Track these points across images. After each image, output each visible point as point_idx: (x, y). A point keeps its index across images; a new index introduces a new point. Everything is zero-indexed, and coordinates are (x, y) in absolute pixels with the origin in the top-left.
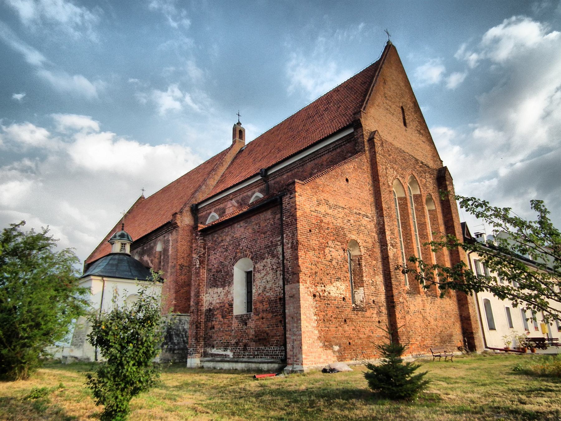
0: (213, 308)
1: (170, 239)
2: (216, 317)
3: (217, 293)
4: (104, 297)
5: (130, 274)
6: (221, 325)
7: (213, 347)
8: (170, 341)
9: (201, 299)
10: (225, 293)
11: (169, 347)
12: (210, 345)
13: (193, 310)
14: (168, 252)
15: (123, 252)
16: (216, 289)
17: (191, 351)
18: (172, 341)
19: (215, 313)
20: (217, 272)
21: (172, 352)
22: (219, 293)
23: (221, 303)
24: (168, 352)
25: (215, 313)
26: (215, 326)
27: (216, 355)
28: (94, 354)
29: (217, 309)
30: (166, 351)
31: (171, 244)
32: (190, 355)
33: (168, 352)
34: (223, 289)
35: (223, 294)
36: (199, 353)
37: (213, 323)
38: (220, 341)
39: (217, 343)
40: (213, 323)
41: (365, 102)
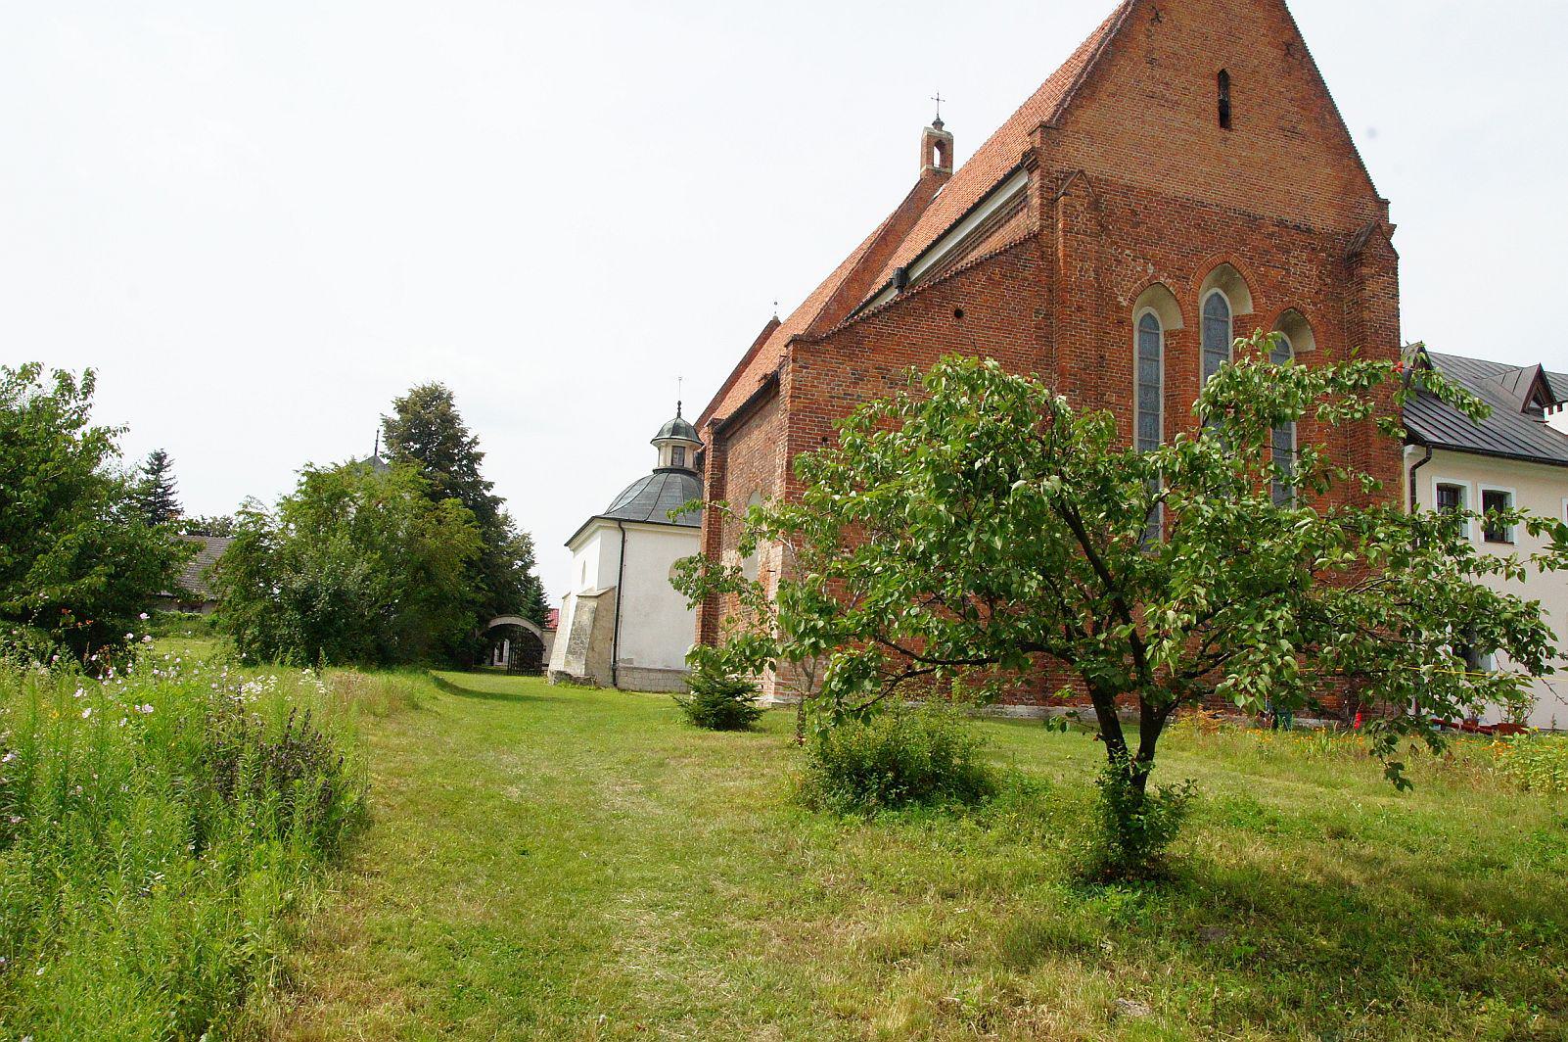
15: (677, 464)
28: (611, 673)
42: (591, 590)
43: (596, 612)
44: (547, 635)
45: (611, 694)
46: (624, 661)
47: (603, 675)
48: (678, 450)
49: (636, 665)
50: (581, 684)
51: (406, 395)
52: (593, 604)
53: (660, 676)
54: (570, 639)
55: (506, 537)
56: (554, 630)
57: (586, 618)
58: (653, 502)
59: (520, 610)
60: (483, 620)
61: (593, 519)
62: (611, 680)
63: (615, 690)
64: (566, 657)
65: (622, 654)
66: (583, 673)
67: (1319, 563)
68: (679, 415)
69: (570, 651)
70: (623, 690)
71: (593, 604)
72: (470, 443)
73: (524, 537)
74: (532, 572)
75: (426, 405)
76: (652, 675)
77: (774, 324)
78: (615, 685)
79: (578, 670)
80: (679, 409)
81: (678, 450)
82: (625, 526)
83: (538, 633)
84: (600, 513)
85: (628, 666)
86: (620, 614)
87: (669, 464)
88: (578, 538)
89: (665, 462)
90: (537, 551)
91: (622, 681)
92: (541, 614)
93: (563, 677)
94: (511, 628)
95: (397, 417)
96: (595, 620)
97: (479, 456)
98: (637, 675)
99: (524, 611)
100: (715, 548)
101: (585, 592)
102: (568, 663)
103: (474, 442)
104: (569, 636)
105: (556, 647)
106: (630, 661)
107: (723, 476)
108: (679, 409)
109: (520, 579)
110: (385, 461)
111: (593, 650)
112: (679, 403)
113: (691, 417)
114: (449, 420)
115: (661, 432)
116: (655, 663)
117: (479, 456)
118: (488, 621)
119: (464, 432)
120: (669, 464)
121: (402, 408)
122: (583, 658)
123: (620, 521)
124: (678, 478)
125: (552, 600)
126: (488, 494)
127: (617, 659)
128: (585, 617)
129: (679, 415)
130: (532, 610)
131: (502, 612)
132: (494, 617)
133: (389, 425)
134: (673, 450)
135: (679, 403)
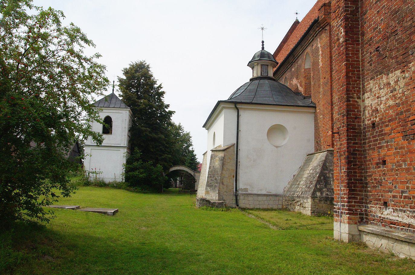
0: (381, 119)
1: (319, 45)
2: (387, 138)
3: (389, 84)
4: (240, 129)
5: (271, 99)
6: (403, 156)
7: (386, 204)
8: (326, 186)
9: (354, 105)
10: (407, 80)
11: (324, 195)
12: (380, 200)
13: (338, 128)
14: (318, 65)
15: (265, 75)
16: (384, 77)
17: (339, 209)
18: (328, 186)
19: (387, 130)
20: (386, 38)
21: (328, 202)
22: (392, 83)
23: (397, 105)
24: (322, 202)
25: (387, 130)
26: (388, 159)
27: (392, 223)
28: (234, 198)
29: (389, 121)
30: (320, 201)
31: (320, 53)
32: (338, 216)
33: (322, 202)
34: (403, 72)
35: (402, 83)
36: (356, 214)
37: (383, 152)
38: (402, 192)
39: (394, 197)
40: (383, 152)
41: (395, 221)
42: (220, 146)
43: (223, 160)
44: (197, 174)
45: (236, 214)
46: (242, 190)
47: (230, 200)
48: (264, 67)
49: (249, 192)
50: (217, 207)
51: (128, 67)
52: (221, 155)
53: (265, 198)
54: (208, 177)
55: (180, 135)
56: (200, 172)
57: (217, 164)
58: (253, 94)
59: (185, 164)
60: (166, 169)
61: (219, 103)
62: (234, 202)
63: (237, 209)
64: (206, 189)
65: (241, 186)
66: (217, 198)
67: (16, 194)
68: (263, 48)
69: (209, 185)
70: (243, 209)
71: (221, 155)
72: (158, 87)
73: (188, 134)
74: (190, 148)
75: (136, 71)
76: (260, 198)
77: (297, 23)
78: (238, 205)
79: (214, 197)
80: (263, 45)
81: (264, 67)
82: (238, 106)
83: (192, 173)
84: (226, 98)
85: (245, 193)
86: (238, 161)
87: (259, 75)
88: (211, 119)
89: (257, 74)
90: (193, 140)
91: (242, 203)
92: (195, 166)
93: (206, 203)
94: (212, 168)
95: (124, 78)
96: (223, 165)
97: (163, 93)
98: (250, 198)
99: (187, 164)
100: (356, 81)
101: (215, 148)
102: (207, 192)
103: (160, 87)
104: (207, 175)
105: (201, 181)
106: (246, 190)
107: (357, 8)
108: (263, 45)
109: (186, 152)
110: (121, 98)
111: (223, 184)
112: (263, 42)
113: (271, 49)
114: (147, 76)
115: (254, 57)
116: (261, 190)
117: (163, 93)
118: (169, 169)
119: (155, 83)
120: (259, 75)
121: (126, 72)
122: (217, 189)
123: (235, 103)
124: (267, 81)
125: (199, 159)
126: (167, 110)
127: (238, 189)
128: (217, 163)
129: (263, 48)
130: (190, 163)
131: (175, 164)
132: (171, 167)
133: (121, 80)
134: (261, 68)
135: (263, 42)
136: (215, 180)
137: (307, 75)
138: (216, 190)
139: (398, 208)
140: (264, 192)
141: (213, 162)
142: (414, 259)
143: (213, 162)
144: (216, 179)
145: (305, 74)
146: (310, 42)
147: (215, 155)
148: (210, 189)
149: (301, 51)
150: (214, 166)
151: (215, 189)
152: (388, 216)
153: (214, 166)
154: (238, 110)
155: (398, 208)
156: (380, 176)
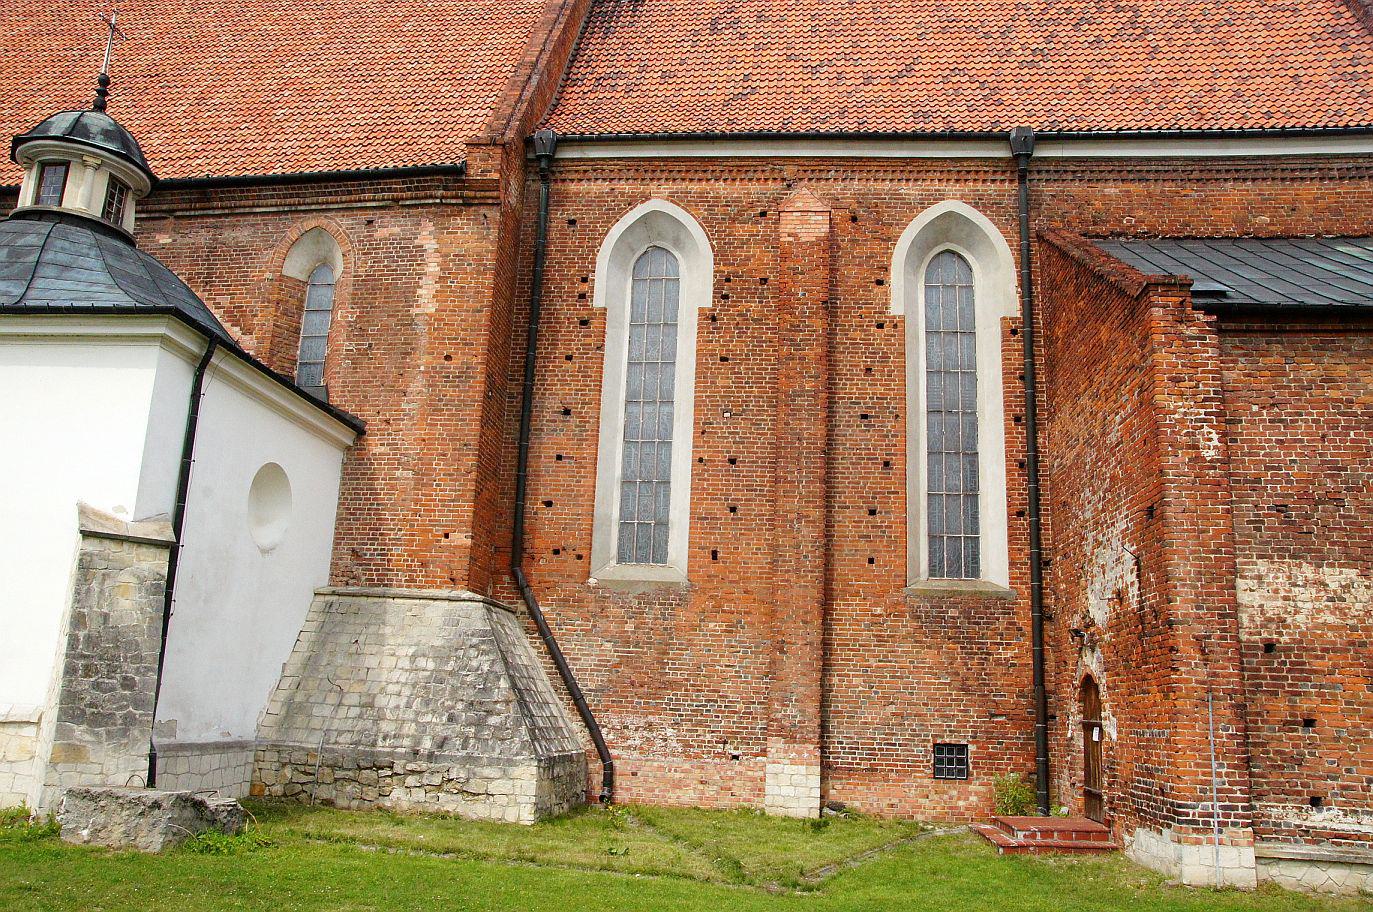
7: (1316, 802)
49: (181, 738)
136: (124, 686)
137: (287, 301)
138: (135, 740)
139: (1360, 809)
140: (213, 736)
141: (102, 592)
142: (1369, 890)
143: (102, 592)
144: (127, 683)
145: (279, 293)
146: (359, 205)
147: (109, 560)
148: (97, 734)
149: (272, 206)
150: (106, 617)
151: (125, 733)
152: (1325, 824)
153: (106, 617)
154: (201, 367)
155: (1360, 809)
156: (1295, 746)
